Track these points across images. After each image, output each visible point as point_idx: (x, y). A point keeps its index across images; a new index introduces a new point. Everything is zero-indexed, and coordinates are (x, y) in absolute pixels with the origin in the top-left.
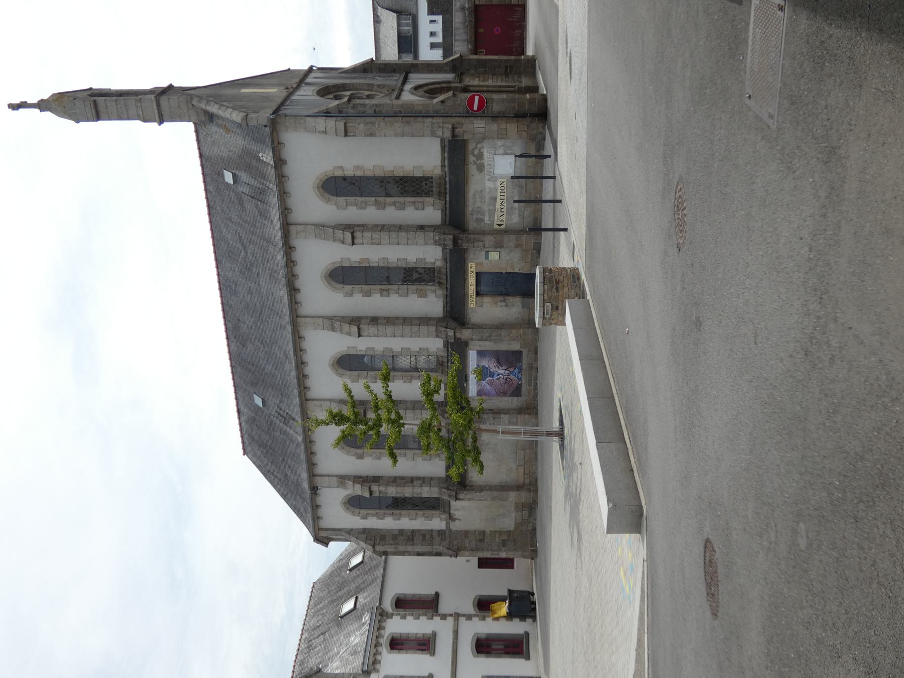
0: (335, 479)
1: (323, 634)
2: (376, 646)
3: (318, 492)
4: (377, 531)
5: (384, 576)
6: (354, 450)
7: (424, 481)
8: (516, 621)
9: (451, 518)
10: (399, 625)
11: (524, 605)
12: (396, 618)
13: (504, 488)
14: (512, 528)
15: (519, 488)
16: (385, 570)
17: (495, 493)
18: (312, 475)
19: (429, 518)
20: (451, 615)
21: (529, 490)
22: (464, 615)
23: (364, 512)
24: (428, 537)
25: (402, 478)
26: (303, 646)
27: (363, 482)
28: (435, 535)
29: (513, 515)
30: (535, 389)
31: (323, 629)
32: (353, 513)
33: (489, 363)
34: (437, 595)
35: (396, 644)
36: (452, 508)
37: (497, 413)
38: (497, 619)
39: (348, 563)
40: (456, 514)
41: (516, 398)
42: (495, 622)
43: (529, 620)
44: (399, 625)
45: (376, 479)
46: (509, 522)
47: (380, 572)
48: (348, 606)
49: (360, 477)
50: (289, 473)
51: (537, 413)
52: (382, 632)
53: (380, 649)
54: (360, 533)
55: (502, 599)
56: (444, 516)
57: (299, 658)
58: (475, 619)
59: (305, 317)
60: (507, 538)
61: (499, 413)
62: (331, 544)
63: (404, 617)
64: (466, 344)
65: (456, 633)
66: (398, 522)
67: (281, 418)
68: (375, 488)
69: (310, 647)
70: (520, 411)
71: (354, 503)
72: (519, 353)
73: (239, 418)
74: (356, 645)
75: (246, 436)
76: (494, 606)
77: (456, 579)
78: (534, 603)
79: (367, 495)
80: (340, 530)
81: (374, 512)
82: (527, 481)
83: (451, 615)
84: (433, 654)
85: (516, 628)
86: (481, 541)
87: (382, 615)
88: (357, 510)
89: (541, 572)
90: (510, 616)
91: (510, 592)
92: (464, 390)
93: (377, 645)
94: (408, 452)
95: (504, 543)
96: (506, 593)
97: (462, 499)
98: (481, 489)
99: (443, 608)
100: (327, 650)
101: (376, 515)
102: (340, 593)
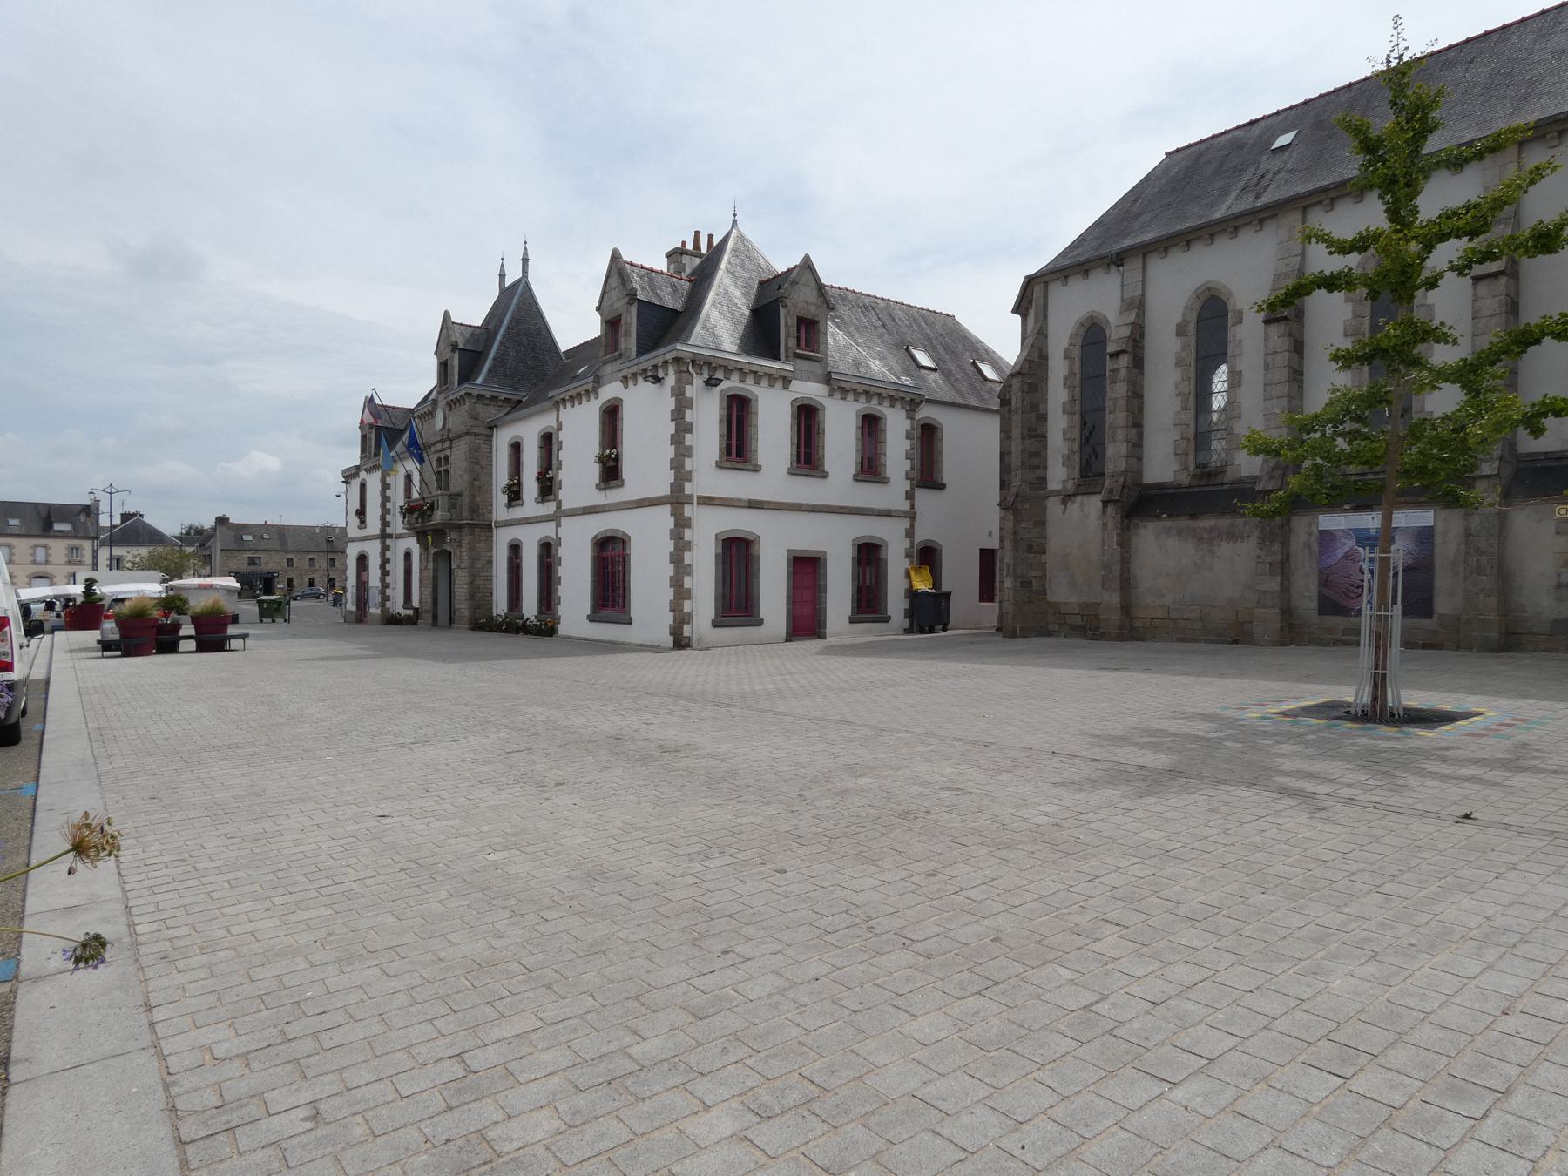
0: (1139, 292)
1: (884, 325)
2: (866, 392)
3: (1113, 268)
4: (1044, 378)
5: (967, 407)
6: (1193, 318)
7: (1137, 446)
8: (905, 604)
9: (1067, 498)
10: (897, 427)
11: (928, 615)
12: (907, 425)
13: (1126, 583)
14: (1051, 598)
15: (1126, 608)
16: (976, 409)
17: (1116, 569)
18: (1145, 251)
19: (1067, 461)
20: (912, 506)
21: (1121, 627)
22: (912, 526)
23: (1077, 352)
24: (1036, 461)
25: (1140, 409)
26: (867, 300)
27: (1134, 340)
28: (1039, 473)
29: (1073, 599)
30: (1336, 643)
31: (890, 325)
32: (1073, 336)
33: (1399, 553)
34: (942, 487)
35: (870, 426)
36: (1085, 498)
37: (1283, 567)
38: (908, 576)
39: (983, 360)
40: (1074, 507)
41: (1314, 604)
42: (903, 573)
43: (906, 623)
44: (897, 427)
45: (1138, 364)
46: (1060, 592)
47: (973, 402)
48: (924, 359)
49: (1142, 336)
50: (1146, 217)
51: (1283, 644)
52: (887, 403)
53: (863, 399)
54: (1041, 350)
55: (936, 584)
56: (1070, 485)
57: (851, 296)
58: (907, 543)
59: (1519, 157)
60: (1032, 588)
61: (1282, 573)
62: (1018, 318)
63: (909, 436)
64: (1450, 501)
65: (887, 514)
66: (1060, 410)
67: (1255, 181)
68: (1124, 361)
69: (865, 309)
70: (1287, 612)
71: (1092, 334)
72: (1428, 613)
73: (1239, 127)
74: (868, 366)
75: (1203, 147)
76: (926, 572)
77: (967, 512)
78: (931, 631)
79: (1111, 348)
80: (1045, 317)
81: (1077, 368)
82: (1138, 624)
83: (912, 506)
84: (857, 478)
85: (896, 603)
86: (1030, 548)
87: (911, 402)
88: (1079, 341)
89: (971, 647)
90: (912, 594)
91: (948, 595)
92: (1333, 505)
93: (868, 395)
94: (1192, 413)
95: (1026, 584)
96: (945, 588)
97: (1104, 512)
98: (1124, 544)
99: (923, 496)
100: (861, 330)
101: (1072, 373)
102: (941, 350)
